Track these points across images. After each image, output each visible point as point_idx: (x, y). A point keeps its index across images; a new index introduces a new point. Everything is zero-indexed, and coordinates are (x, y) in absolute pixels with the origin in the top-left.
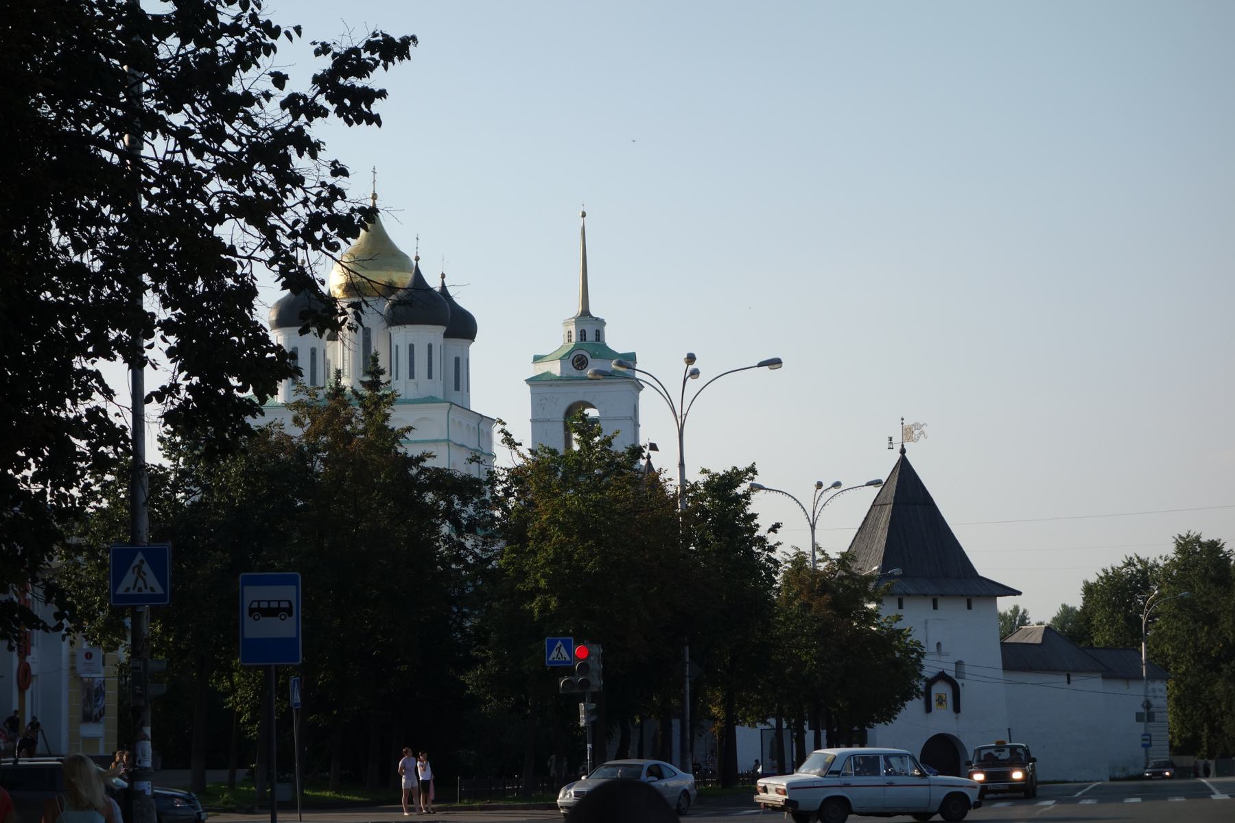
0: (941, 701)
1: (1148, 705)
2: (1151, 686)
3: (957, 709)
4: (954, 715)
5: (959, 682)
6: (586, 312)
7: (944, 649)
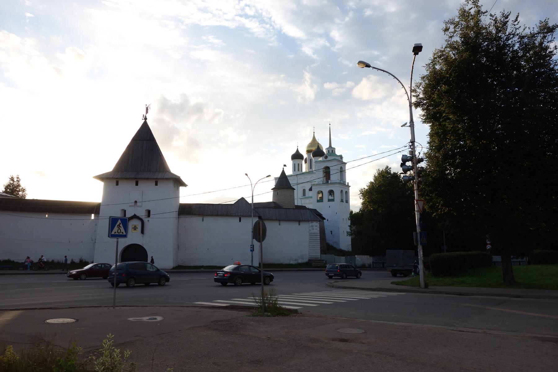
0: (135, 228)
2: (311, 224)
3: (142, 232)
4: (142, 235)
5: (145, 220)
6: (330, 146)
7: (138, 204)
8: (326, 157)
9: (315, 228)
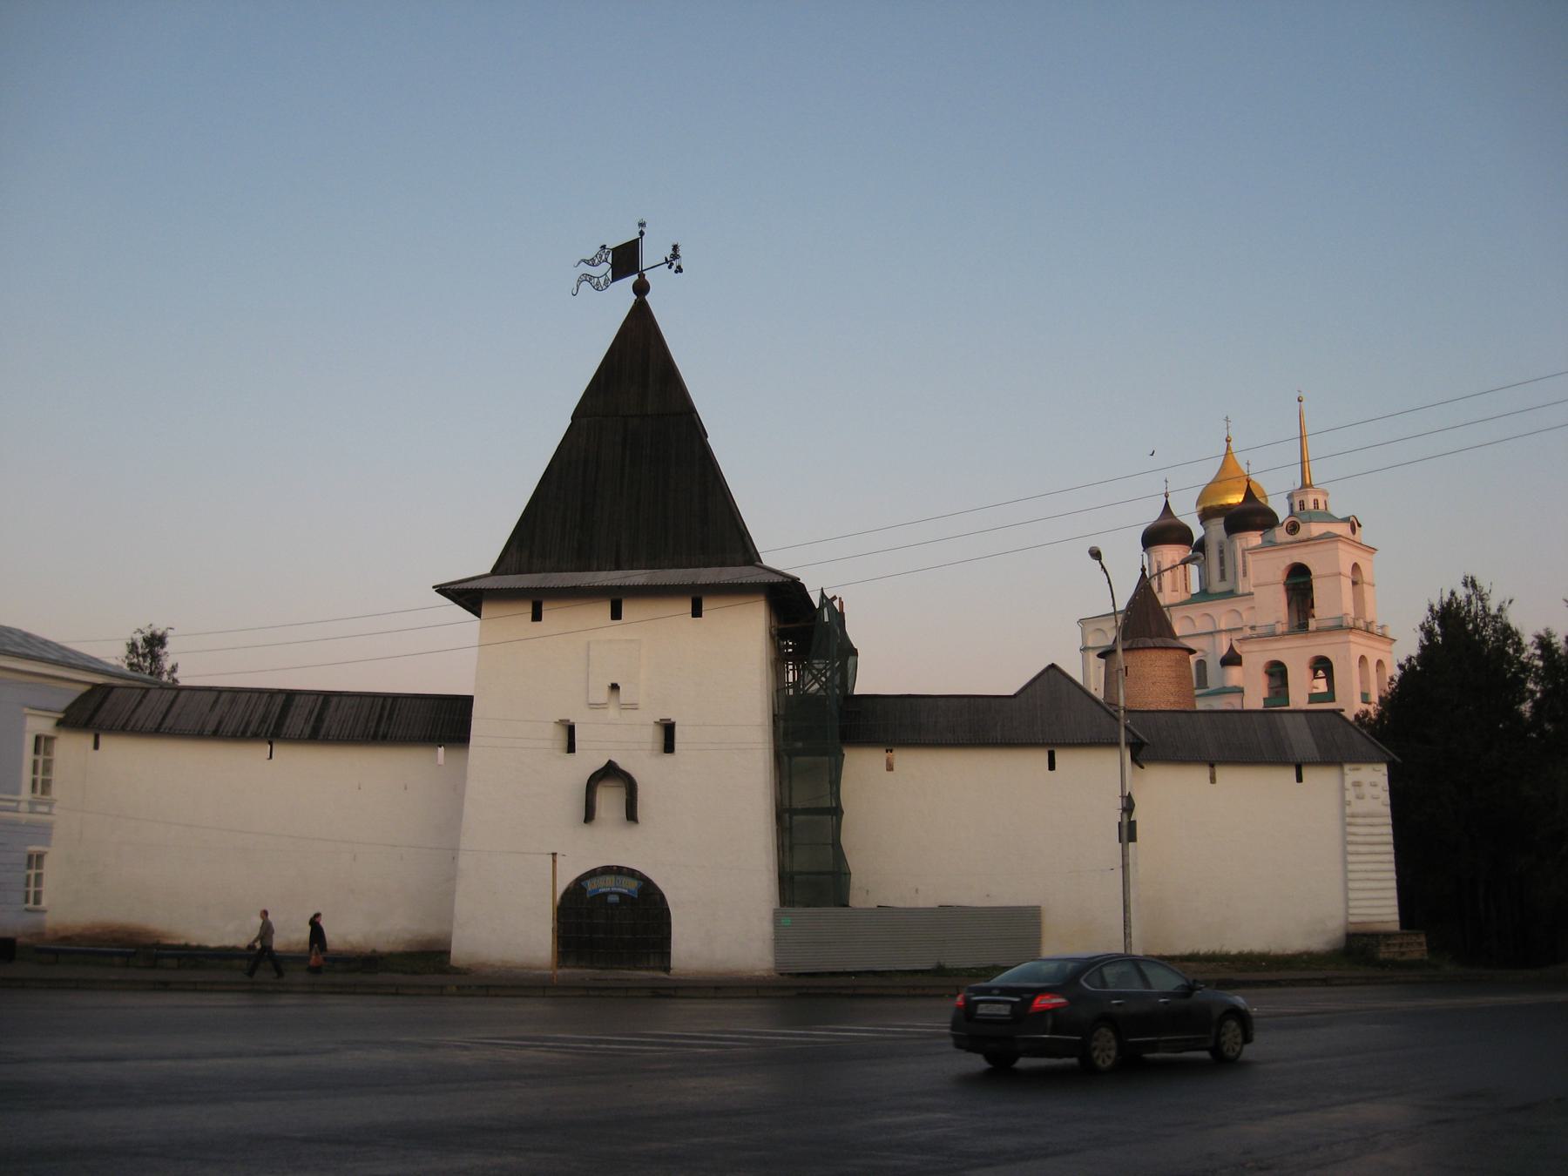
3: (631, 815)
8: (1293, 528)
9: (1367, 790)
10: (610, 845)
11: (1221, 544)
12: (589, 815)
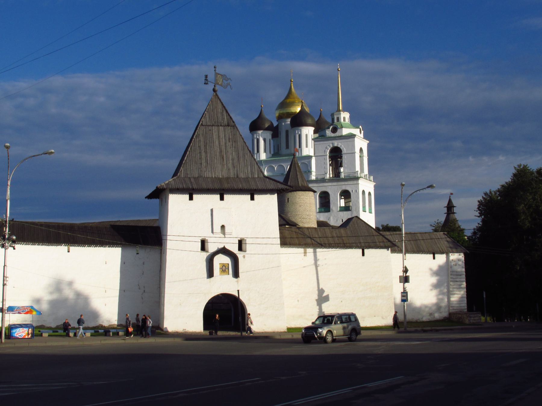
1: (406, 270)
3: (236, 274)
5: (240, 255)
7: (227, 230)
10: (223, 284)
11: (287, 132)
12: (210, 274)
